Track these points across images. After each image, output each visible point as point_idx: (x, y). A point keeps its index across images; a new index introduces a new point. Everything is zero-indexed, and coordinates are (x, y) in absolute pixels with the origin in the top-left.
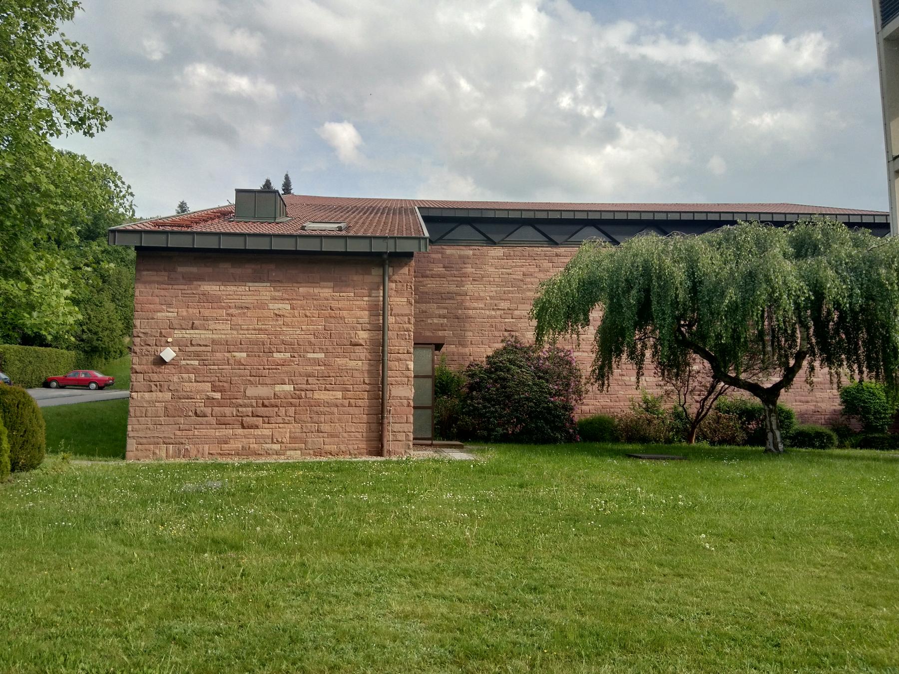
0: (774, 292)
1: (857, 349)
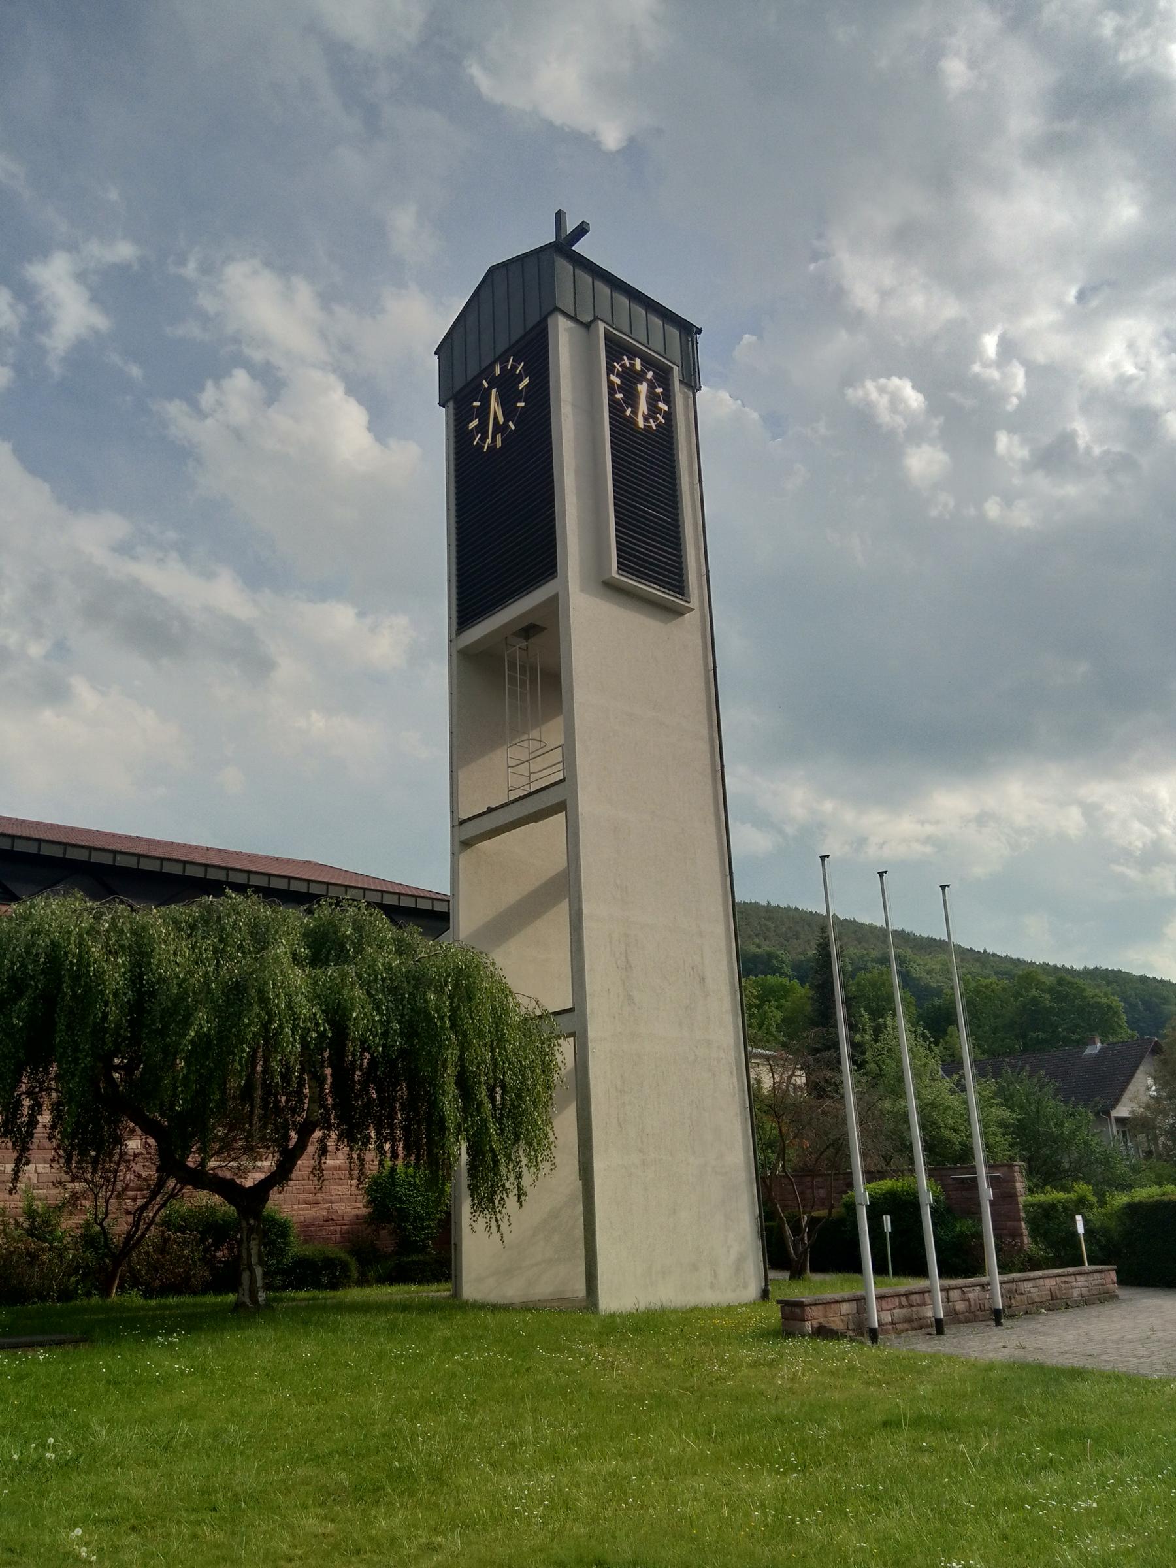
0: (270, 1021)
1: (392, 1116)
